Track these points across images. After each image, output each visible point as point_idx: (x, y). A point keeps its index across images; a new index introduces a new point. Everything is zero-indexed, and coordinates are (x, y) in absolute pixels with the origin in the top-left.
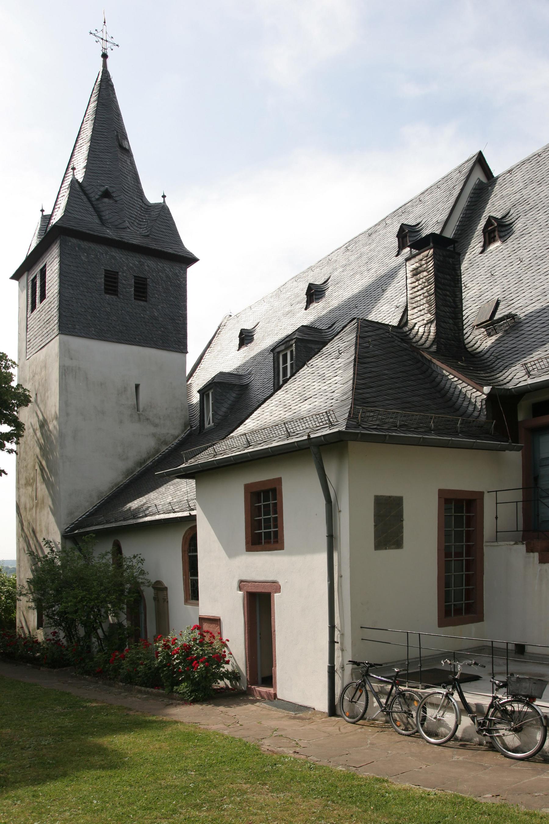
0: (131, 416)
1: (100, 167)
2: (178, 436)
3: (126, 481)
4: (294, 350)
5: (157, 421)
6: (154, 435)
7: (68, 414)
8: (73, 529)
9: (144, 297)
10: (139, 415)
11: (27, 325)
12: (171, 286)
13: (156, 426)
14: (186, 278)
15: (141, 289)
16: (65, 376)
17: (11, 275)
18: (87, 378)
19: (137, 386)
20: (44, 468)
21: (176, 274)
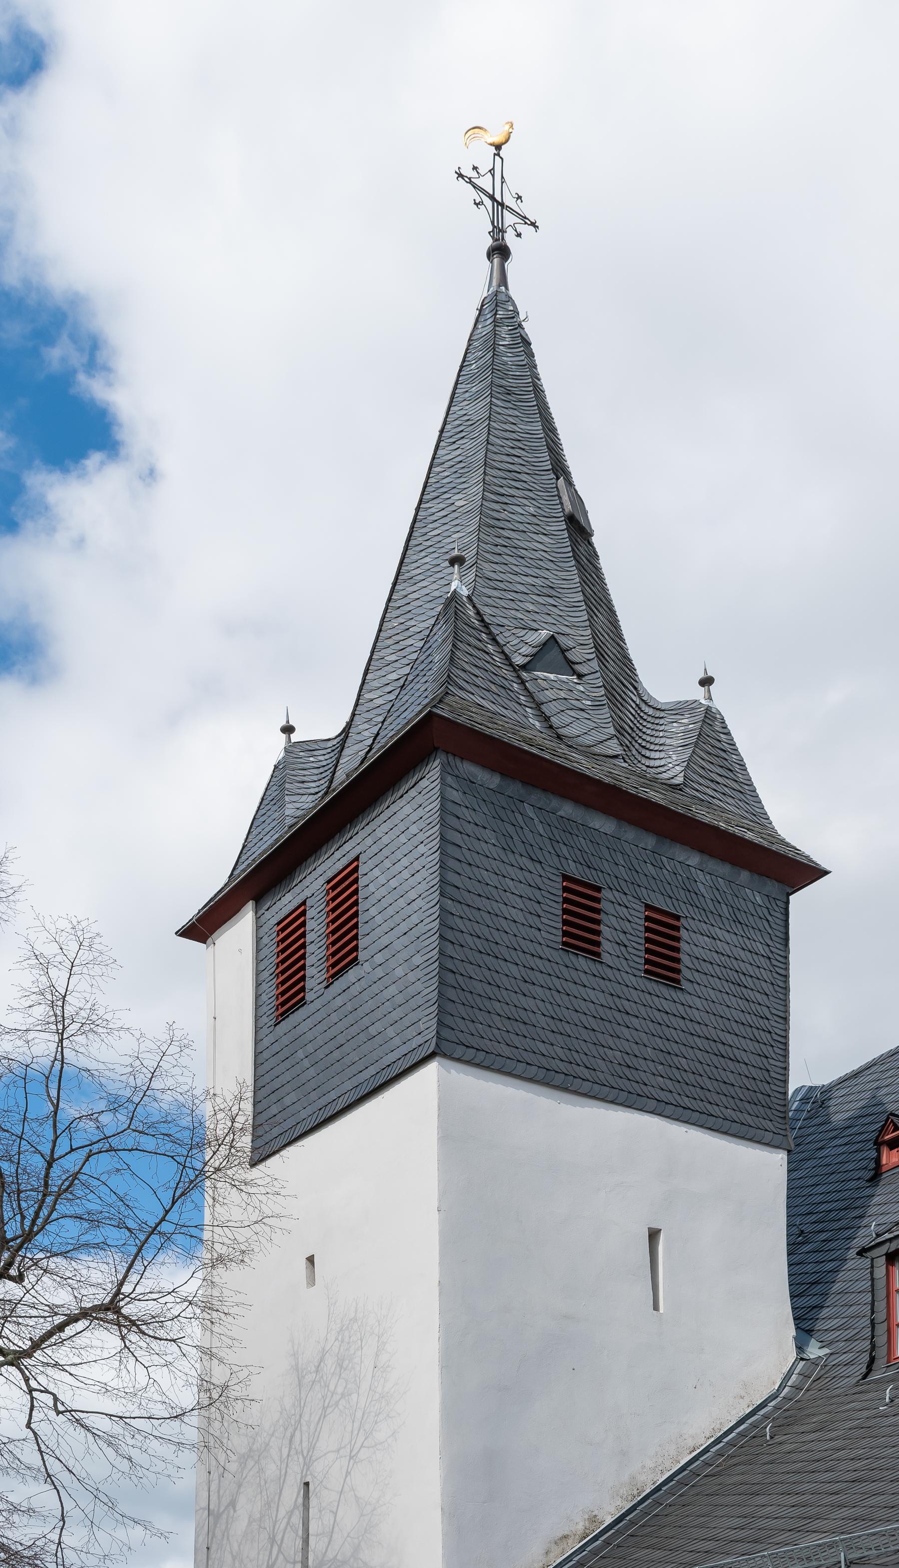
15: (663, 957)
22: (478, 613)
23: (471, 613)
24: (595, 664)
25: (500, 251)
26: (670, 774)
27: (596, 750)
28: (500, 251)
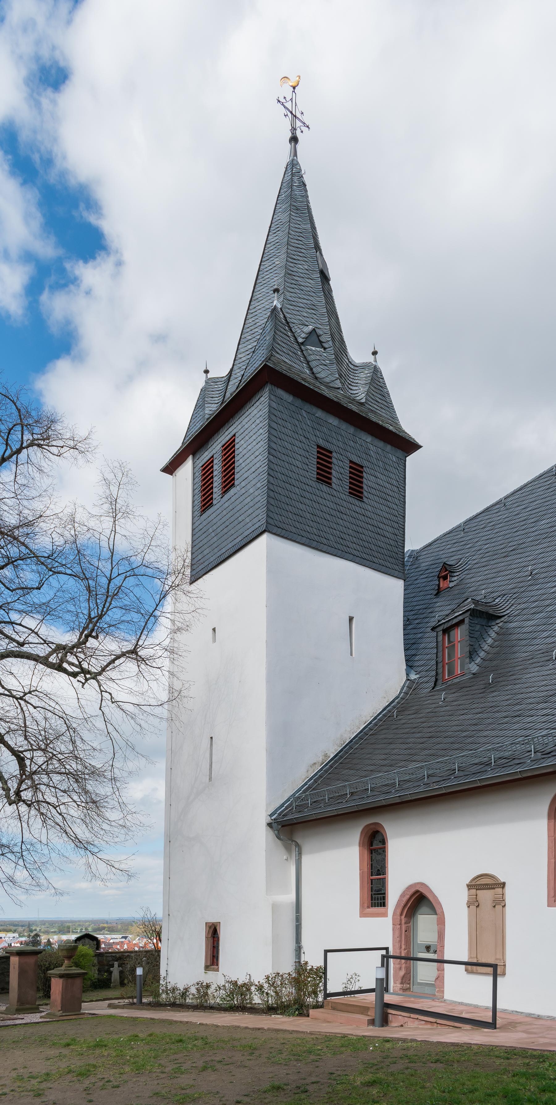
1: (300, 298)
22: (285, 317)
23: (282, 316)
24: (331, 343)
25: (294, 139)
27: (331, 385)
28: (294, 139)
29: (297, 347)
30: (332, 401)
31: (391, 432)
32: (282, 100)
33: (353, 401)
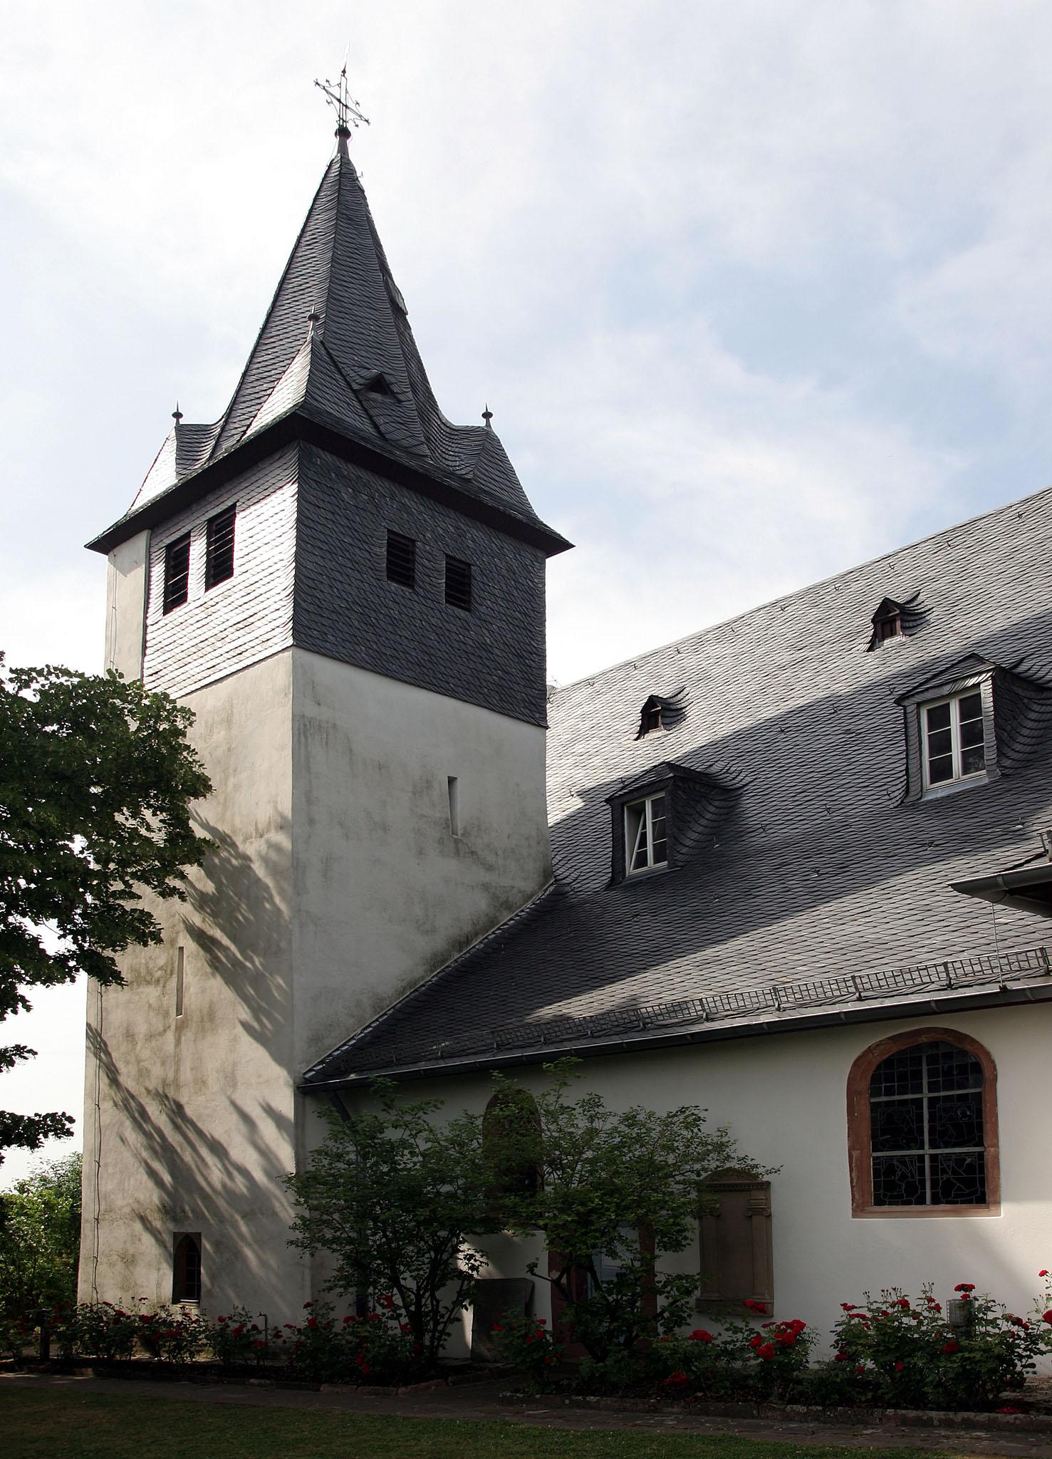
0: (441, 841)
2: (530, 897)
3: (432, 977)
4: (987, 701)
5: (491, 859)
6: (485, 887)
7: (311, 822)
8: (324, 1074)
9: (464, 601)
10: (456, 841)
11: (145, 641)
12: (517, 589)
13: (490, 868)
14: (544, 578)
15: (460, 586)
16: (306, 738)
17: (93, 536)
18: (351, 750)
19: (451, 781)
20: (213, 941)
21: (525, 567)
22: (329, 353)
23: (323, 352)
24: (410, 395)
25: (343, 133)
26: (463, 472)
27: (413, 450)
28: (343, 133)
29: (351, 395)
30: (416, 472)
31: (520, 521)
32: (323, 83)
33: (452, 475)
